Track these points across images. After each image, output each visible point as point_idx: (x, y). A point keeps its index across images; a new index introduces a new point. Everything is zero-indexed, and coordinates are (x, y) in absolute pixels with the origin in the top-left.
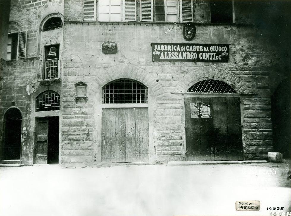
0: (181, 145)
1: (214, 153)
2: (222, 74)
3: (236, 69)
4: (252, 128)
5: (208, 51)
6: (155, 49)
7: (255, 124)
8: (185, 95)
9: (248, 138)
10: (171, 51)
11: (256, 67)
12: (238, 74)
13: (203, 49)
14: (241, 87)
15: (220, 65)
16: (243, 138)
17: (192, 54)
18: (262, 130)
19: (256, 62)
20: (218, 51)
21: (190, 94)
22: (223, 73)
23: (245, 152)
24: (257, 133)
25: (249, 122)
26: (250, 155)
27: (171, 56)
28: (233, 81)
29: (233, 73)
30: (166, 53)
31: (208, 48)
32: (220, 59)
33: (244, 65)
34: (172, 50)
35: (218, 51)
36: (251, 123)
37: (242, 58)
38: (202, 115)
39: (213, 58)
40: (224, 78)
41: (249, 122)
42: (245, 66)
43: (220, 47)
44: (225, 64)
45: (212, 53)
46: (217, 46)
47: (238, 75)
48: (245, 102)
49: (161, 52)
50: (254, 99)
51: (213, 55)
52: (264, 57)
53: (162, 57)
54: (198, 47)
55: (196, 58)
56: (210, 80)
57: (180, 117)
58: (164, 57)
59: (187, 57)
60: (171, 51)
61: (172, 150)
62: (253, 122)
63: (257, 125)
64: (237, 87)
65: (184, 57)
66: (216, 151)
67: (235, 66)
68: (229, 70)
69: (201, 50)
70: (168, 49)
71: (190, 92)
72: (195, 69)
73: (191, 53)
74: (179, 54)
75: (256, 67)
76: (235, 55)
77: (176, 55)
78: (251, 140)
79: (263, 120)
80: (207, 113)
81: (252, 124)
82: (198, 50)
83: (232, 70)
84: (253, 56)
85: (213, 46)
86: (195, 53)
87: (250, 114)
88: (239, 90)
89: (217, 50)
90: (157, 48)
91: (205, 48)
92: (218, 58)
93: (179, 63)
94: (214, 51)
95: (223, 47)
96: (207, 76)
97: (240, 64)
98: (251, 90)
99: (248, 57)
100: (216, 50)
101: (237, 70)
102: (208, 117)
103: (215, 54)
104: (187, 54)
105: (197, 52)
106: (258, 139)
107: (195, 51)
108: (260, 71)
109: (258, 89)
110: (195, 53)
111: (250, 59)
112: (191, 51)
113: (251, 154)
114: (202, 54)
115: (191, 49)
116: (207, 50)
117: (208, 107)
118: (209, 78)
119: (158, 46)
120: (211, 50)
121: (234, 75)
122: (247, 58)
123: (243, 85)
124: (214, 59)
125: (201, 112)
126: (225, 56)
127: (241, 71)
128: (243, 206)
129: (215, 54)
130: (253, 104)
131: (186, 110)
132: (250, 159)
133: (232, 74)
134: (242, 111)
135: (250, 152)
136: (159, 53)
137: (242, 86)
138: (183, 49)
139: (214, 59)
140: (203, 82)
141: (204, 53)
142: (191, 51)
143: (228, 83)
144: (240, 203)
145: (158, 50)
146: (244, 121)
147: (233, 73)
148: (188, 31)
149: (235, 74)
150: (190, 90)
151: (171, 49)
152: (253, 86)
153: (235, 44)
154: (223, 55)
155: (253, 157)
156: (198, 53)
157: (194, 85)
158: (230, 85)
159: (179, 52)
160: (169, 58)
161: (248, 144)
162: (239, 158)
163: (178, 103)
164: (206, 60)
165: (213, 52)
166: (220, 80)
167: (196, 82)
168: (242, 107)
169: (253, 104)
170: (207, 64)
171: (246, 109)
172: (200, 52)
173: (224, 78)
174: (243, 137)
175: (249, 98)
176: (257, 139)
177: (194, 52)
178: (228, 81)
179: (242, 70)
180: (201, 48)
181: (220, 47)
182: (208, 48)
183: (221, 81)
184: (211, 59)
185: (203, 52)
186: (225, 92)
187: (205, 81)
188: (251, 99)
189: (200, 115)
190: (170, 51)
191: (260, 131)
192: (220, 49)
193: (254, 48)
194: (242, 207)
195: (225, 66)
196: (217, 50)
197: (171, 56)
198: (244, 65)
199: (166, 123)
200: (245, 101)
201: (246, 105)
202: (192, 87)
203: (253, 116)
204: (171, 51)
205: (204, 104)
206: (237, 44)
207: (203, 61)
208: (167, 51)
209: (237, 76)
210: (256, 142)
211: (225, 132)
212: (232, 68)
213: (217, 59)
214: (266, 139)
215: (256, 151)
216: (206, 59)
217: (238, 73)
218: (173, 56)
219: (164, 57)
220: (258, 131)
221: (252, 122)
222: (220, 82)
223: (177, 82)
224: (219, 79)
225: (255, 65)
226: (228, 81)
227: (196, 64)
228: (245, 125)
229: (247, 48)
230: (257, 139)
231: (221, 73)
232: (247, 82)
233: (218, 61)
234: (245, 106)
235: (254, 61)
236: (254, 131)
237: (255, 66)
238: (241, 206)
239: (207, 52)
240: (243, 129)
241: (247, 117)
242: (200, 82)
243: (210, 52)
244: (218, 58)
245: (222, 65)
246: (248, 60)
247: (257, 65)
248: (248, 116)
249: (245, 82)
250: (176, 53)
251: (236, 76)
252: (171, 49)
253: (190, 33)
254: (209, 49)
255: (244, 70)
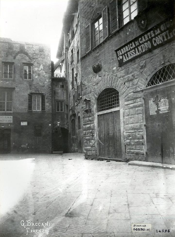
0: (143, 144)
6: (119, 55)
8: (144, 92)
10: (129, 50)
13: (154, 33)
27: (130, 55)
30: (126, 54)
34: (129, 49)
38: (159, 110)
45: (165, 32)
49: (122, 55)
53: (125, 60)
54: (149, 34)
55: (150, 47)
56: (167, 66)
57: (141, 115)
58: (126, 59)
59: (142, 50)
60: (129, 50)
61: (137, 150)
65: (140, 52)
69: (153, 35)
70: (127, 50)
71: (153, 85)
72: (152, 59)
73: (145, 44)
74: (135, 50)
77: (134, 53)
82: (150, 37)
90: (119, 53)
93: (139, 59)
103: (167, 31)
104: (141, 47)
110: (149, 42)
112: (144, 42)
115: (144, 40)
119: (119, 52)
124: (169, 38)
131: (146, 107)
136: (122, 57)
138: (137, 43)
141: (156, 37)
142: (144, 42)
145: (120, 55)
148: (141, 21)
150: (148, 85)
151: (128, 49)
156: (150, 40)
159: (134, 48)
160: (130, 58)
163: (139, 101)
165: (165, 31)
172: (152, 38)
177: (147, 42)
180: (152, 34)
184: (166, 40)
187: (161, 69)
189: (158, 111)
190: (128, 51)
197: (130, 55)
199: (131, 122)
204: (129, 51)
208: (127, 52)
218: (132, 54)
219: (126, 59)
223: (138, 79)
243: (162, 32)
250: (133, 50)
252: (128, 49)
253: (143, 21)
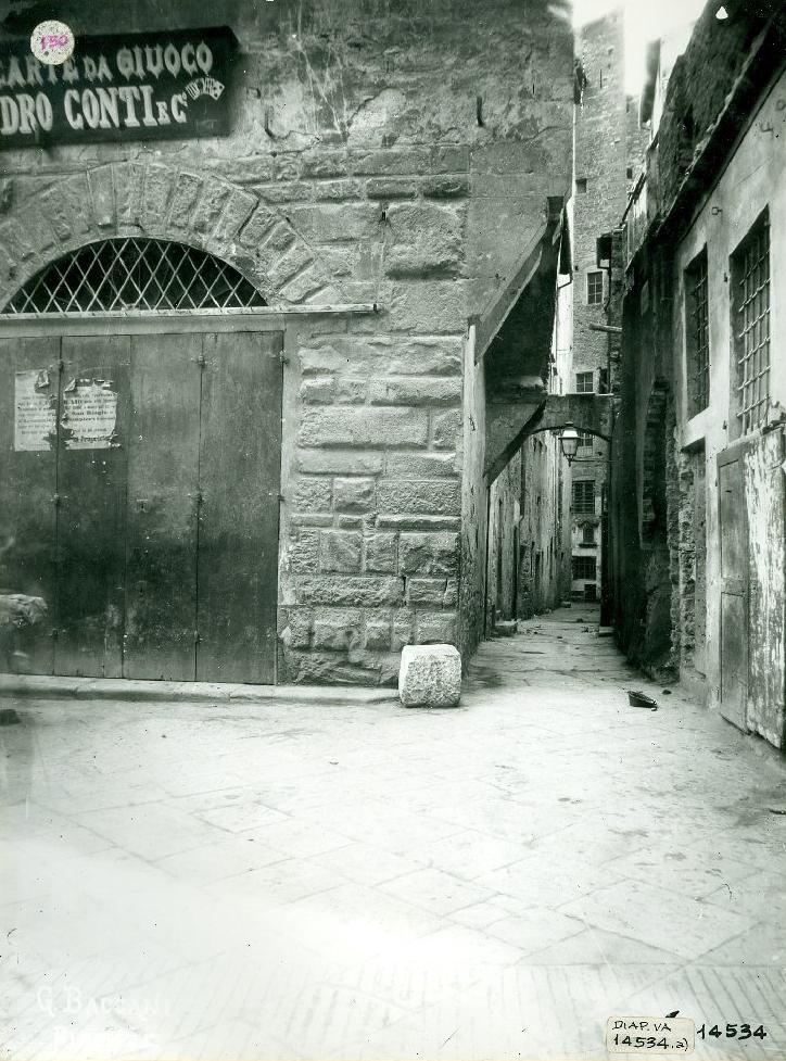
1: (120, 642)
2: (192, 205)
3: (279, 169)
4: (341, 509)
5: (109, 76)
7: (358, 486)
9: (309, 565)
11: (395, 149)
12: (287, 201)
14: (294, 275)
15: (186, 154)
16: (280, 563)
17: (22, 105)
18: (397, 518)
19: (405, 121)
20: (165, 73)
21: (28, 322)
22: (198, 195)
23: (287, 641)
24: (366, 533)
25: (324, 474)
26: (315, 656)
28: (251, 243)
29: (256, 193)
31: (103, 60)
32: (181, 118)
33: (326, 142)
35: (165, 73)
36: (337, 479)
37: (313, 107)
38: (68, 434)
39: (140, 114)
40: (201, 228)
41: (324, 474)
42: (331, 150)
43: (171, 48)
44: (213, 144)
45: (134, 89)
46: (142, 46)
47: (285, 207)
48: (310, 359)
50: (364, 339)
51: (138, 97)
52: (443, 88)
55: (47, 124)
62: (348, 475)
63: (366, 488)
64: (271, 273)
66: (131, 629)
67: (274, 154)
68: (237, 178)
73: (20, 97)
75: (395, 149)
76: (278, 92)
78: (324, 572)
79: (406, 460)
80: (96, 424)
81: (341, 483)
83: (250, 176)
84: (382, 86)
85: (130, 47)
86: (42, 96)
87: (332, 425)
88: (283, 291)
89: (156, 70)
91: (88, 61)
92: (169, 112)
94: (140, 72)
95: (188, 48)
96: (107, 220)
97: (302, 140)
98: (353, 288)
99: (350, 96)
100: (150, 67)
101: (279, 177)
102: (104, 445)
103: (147, 90)
105: (47, 88)
106: (370, 572)
107: (37, 85)
108: (416, 177)
109: (391, 284)
111: (363, 106)
113: (325, 649)
114: (77, 98)
116: (104, 70)
117: (105, 392)
118: (120, 228)
120: (125, 72)
121: (262, 205)
122: (346, 103)
123: (307, 263)
124: (149, 120)
125: (66, 420)
126: (205, 99)
127: (305, 183)
128: (634, 1033)
129: (147, 90)
130: (361, 372)
132: (311, 680)
133: (252, 199)
134: (290, 412)
135: (316, 642)
137: (302, 268)
139: (149, 120)
140: (85, 255)
143: (219, 254)
144: (619, 1024)
146: (298, 470)
147: (256, 193)
149: (269, 202)
152: (367, 263)
153: (282, 25)
154: (197, 94)
155: (327, 665)
157: (40, 273)
158: (232, 264)
161: (306, 597)
162: (254, 673)
164: (107, 129)
165: (134, 81)
166: (178, 237)
167: (53, 257)
168: (293, 387)
169: (361, 372)
170: (116, 153)
171: (313, 399)
172: (64, 86)
173: (201, 228)
174: (283, 557)
175: (334, 338)
176: (364, 568)
177: (32, 90)
178: (220, 240)
179: (311, 176)
181: (171, 48)
182: (103, 60)
183: (186, 247)
185: (81, 84)
186: (49, 311)
187: (97, 246)
188: (348, 338)
189: (60, 437)
191: (385, 526)
192: (173, 62)
193: (389, 41)
194: (627, 1041)
195: (211, 155)
196: (156, 70)
198: (326, 142)
200: (315, 352)
201: (309, 373)
202: (29, 286)
203: (347, 438)
205: (87, 375)
206: (295, 26)
207: (88, 136)
209: (279, 211)
210: (354, 585)
211: (188, 528)
212: (248, 167)
213: (164, 119)
214: (412, 573)
215: (349, 634)
216: (105, 123)
217: (285, 192)
220: (372, 522)
221: (338, 474)
222: (176, 250)
224: (173, 231)
225: (389, 141)
226: (220, 240)
227: (52, 157)
228: (298, 488)
229: (351, 45)
230: (364, 568)
231: (180, 200)
232: (334, 242)
233: (170, 133)
234: (309, 382)
235: (384, 118)
236: (346, 526)
237: (390, 147)
238: (623, 1033)
239: (106, 84)
240: (289, 514)
241: (317, 447)
242: (74, 253)
243: (119, 80)
244: (169, 112)
245: (197, 154)
246: (347, 115)
247: (402, 139)
248: (319, 436)
249: (323, 243)
251: (271, 210)
254: (113, 67)
255: (322, 176)
